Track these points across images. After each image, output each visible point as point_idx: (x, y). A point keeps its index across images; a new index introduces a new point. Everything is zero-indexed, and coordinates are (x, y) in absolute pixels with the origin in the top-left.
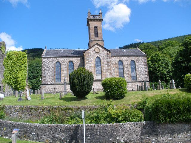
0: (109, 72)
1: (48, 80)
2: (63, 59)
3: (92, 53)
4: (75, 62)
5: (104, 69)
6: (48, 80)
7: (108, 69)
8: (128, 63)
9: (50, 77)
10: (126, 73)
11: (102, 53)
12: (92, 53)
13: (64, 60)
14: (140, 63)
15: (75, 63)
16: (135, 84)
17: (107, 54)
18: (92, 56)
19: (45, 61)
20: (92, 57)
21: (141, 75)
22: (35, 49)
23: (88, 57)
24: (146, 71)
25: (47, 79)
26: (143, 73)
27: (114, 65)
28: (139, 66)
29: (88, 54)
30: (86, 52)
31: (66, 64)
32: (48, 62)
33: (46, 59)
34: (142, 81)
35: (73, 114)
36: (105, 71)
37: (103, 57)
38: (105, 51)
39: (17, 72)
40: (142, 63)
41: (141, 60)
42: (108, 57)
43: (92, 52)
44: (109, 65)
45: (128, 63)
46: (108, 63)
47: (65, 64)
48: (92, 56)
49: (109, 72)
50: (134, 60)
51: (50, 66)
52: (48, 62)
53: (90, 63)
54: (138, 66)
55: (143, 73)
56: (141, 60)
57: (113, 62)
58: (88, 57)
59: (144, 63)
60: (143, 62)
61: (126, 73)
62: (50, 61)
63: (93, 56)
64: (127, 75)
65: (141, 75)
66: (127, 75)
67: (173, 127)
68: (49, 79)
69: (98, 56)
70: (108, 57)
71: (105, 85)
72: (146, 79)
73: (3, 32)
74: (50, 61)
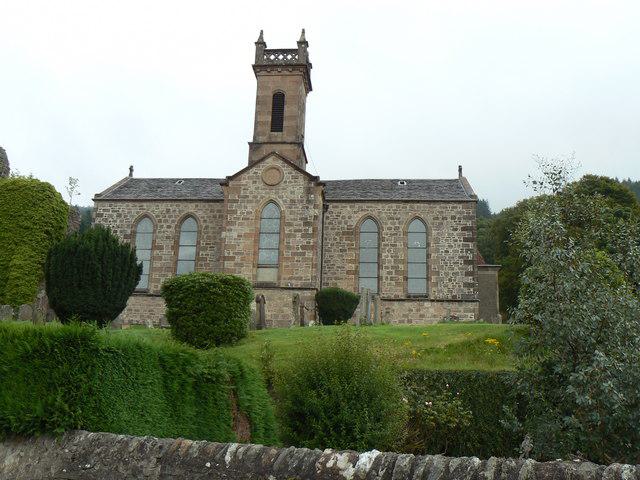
0: (305, 260)
3: (252, 187)
5: (289, 248)
7: (303, 247)
8: (397, 228)
10: (387, 268)
11: (290, 189)
12: (252, 187)
13: (168, 211)
14: (445, 230)
16: (418, 310)
17: (308, 191)
20: (251, 202)
21: (447, 274)
23: (236, 201)
24: (467, 262)
26: (456, 269)
27: (344, 233)
28: (443, 242)
29: (237, 189)
30: (231, 183)
31: (173, 225)
32: (111, 216)
34: (450, 298)
36: (294, 254)
37: (293, 201)
39: (14, 246)
40: (456, 230)
41: (453, 218)
42: (309, 201)
43: (255, 182)
44: (310, 231)
45: (397, 228)
46: (307, 224)
47: (169, 227)
48: (250, 198)
49: (305, 260)
52: (111, 216)
53: (241, 224)
54: (437, 241)
55: (456, 269)
56: (453, 218)
57: (340, 223)
58: (236, 201)
59: (463, 229)
60: (459, 227)
61: (387, 268)
62: (119, 216)
63: (255, 197)
64: (389, 273)
65: (447, 274)
66: (389, 273)
69: (273, 196)
70: (309, 201)
71: (173, 292)
72: (466, 291)
73: (499, 214)
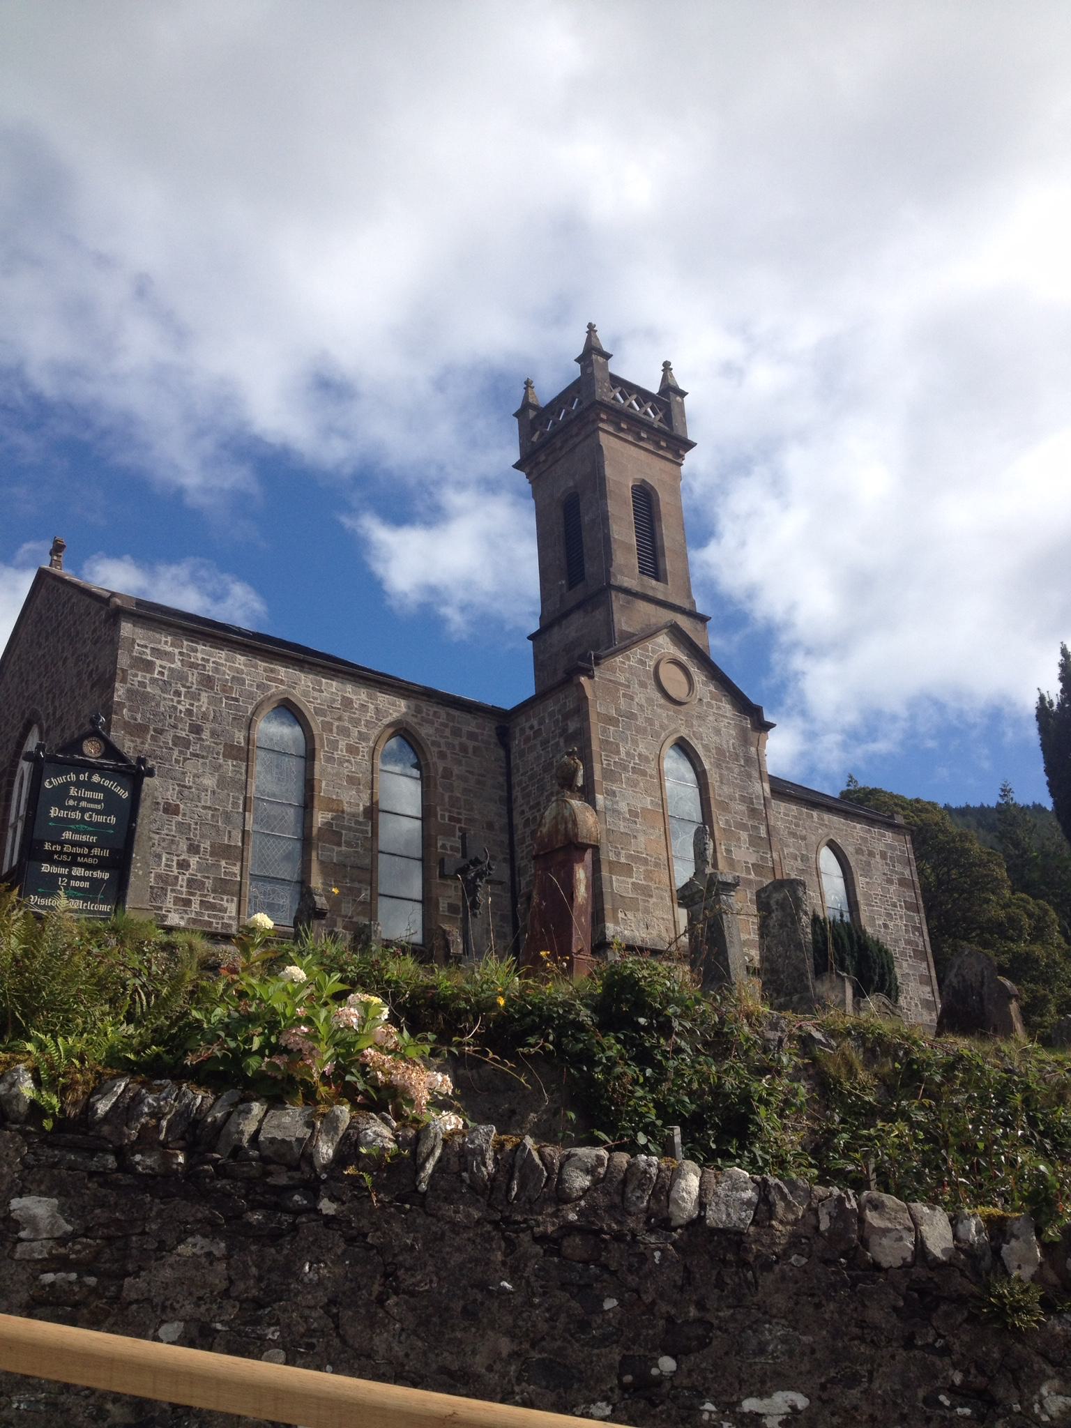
1: (166, 881)
2: (332, 687)
4: (442, 755)
6: (166, 881)
9: (193, 849)
15: (441, 766)
18: (640, 722)
19: (149, 666)
20: (640, 730)
22: (1048, 771)
25: (162, 869)
31: (364, 747)
32: (182, 678)
33: (165, 642)
35: (454, 1163)
38: (727, 708)
50: (839, 841)
51: (206, 735)
67: (880, 1021)
68: (183, 865)
74: (207, 682)
